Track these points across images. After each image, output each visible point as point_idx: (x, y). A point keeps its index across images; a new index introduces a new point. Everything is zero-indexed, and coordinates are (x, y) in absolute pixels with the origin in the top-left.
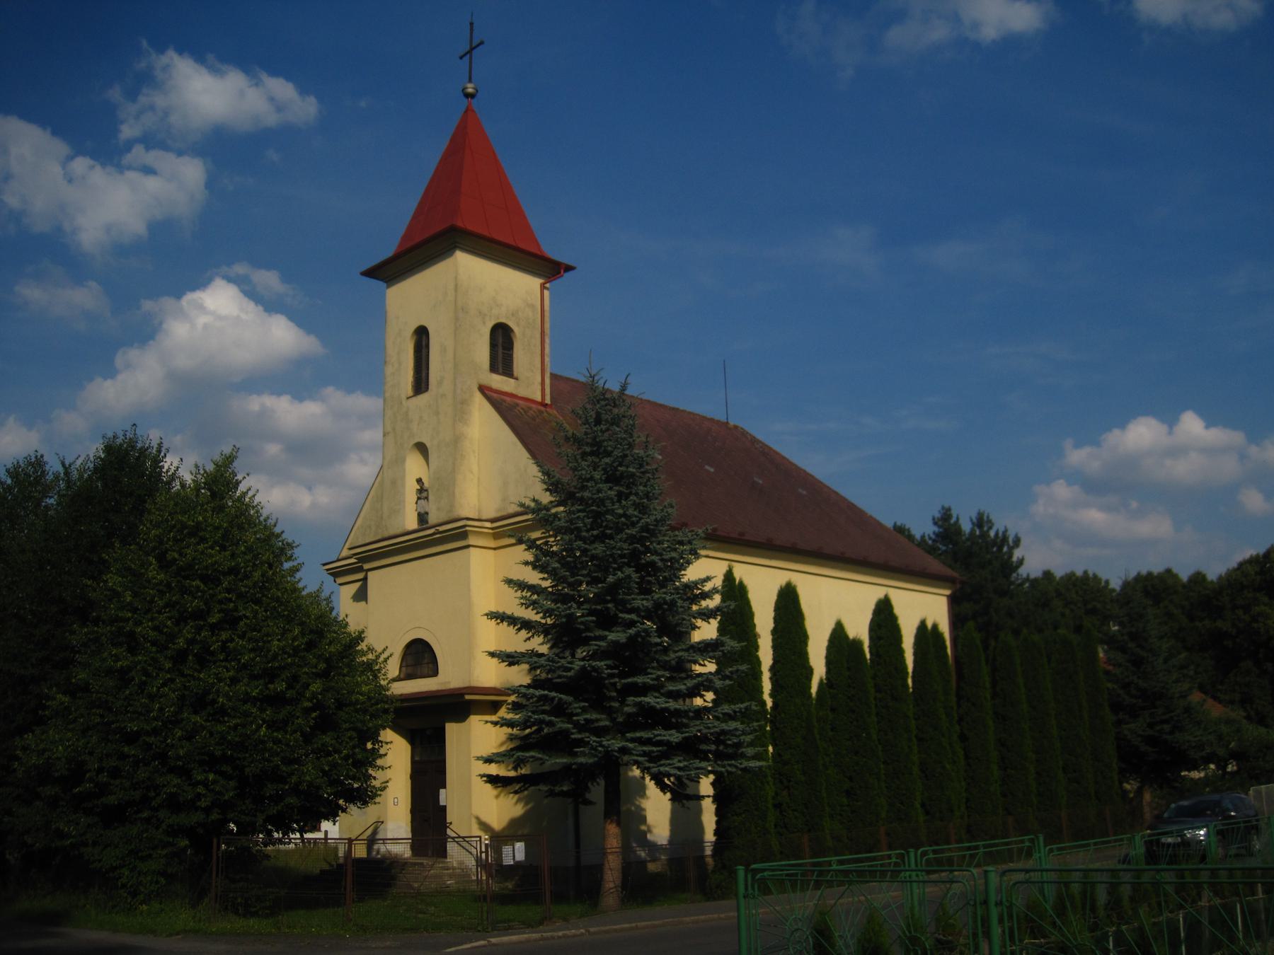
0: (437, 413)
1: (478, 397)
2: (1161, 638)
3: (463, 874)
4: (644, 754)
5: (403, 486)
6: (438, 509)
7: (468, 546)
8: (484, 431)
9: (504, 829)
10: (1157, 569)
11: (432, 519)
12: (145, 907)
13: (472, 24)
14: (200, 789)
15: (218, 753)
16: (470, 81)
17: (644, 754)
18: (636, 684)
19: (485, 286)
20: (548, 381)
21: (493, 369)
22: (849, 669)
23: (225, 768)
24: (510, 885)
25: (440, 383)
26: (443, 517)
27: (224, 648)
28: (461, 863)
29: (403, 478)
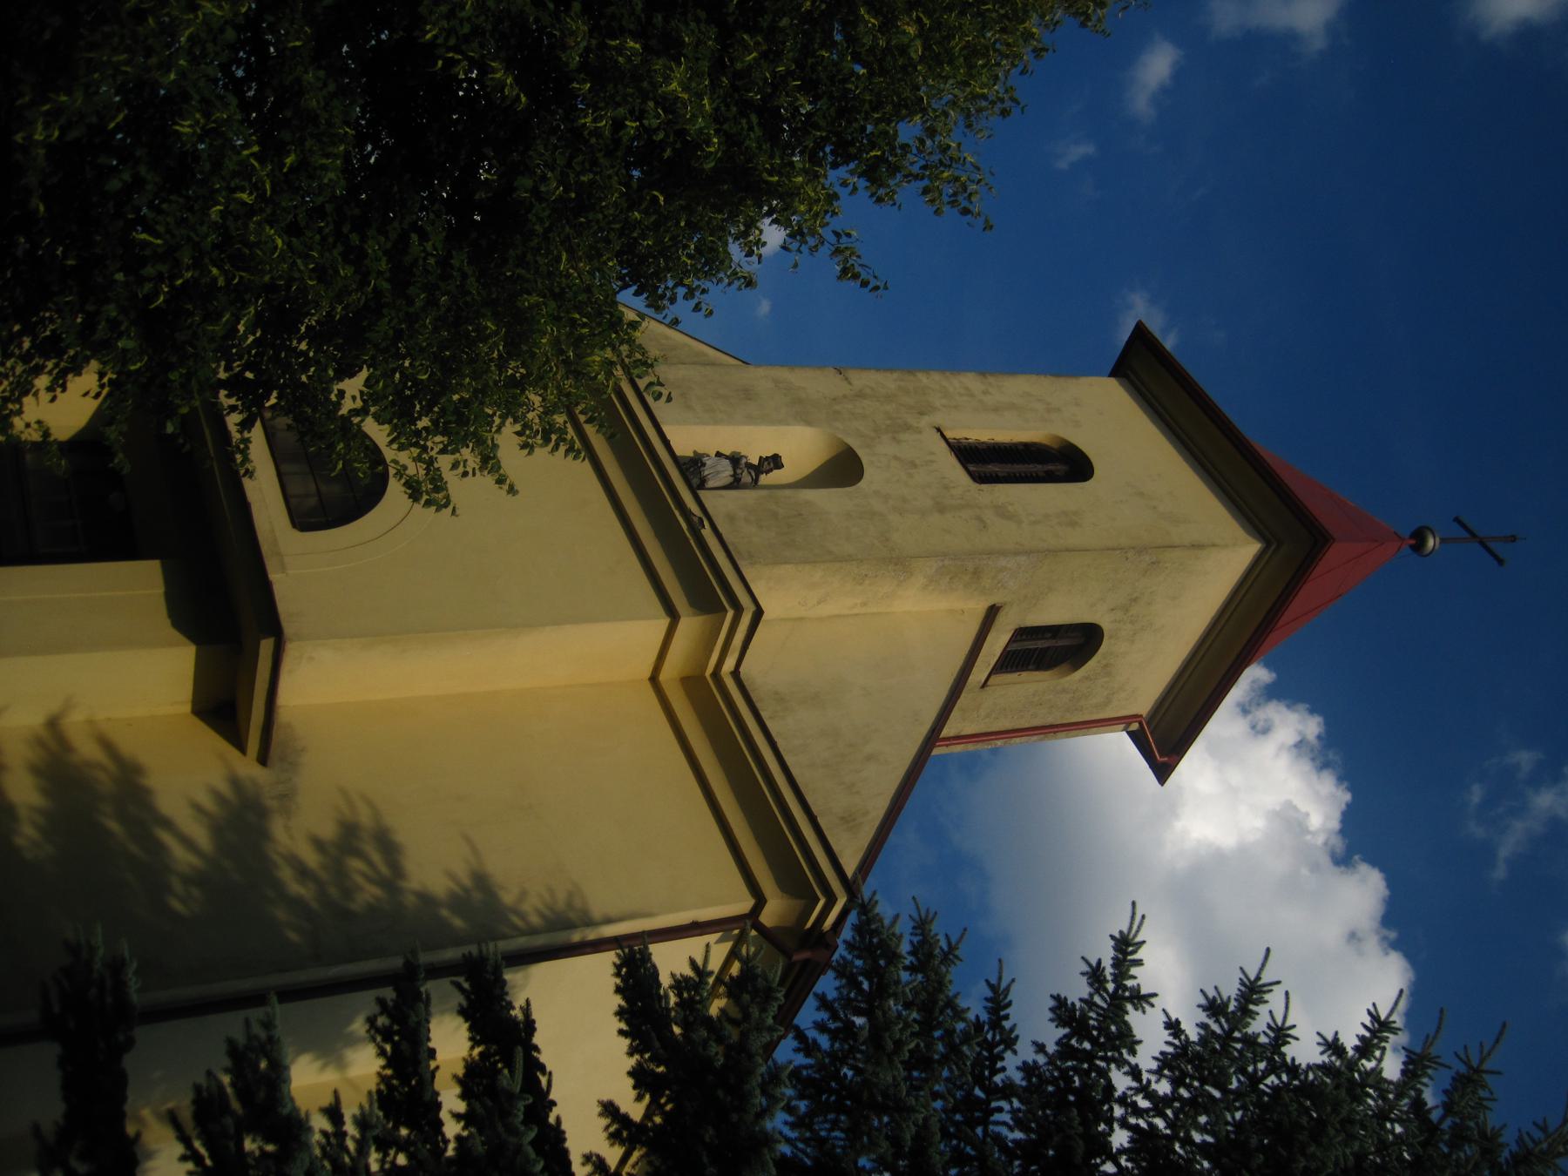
0: (941, 509)
1: (979, 607)
5: (750, 420)
7: (673, 614)
16: (1443, 541)
25: (1002, 512)
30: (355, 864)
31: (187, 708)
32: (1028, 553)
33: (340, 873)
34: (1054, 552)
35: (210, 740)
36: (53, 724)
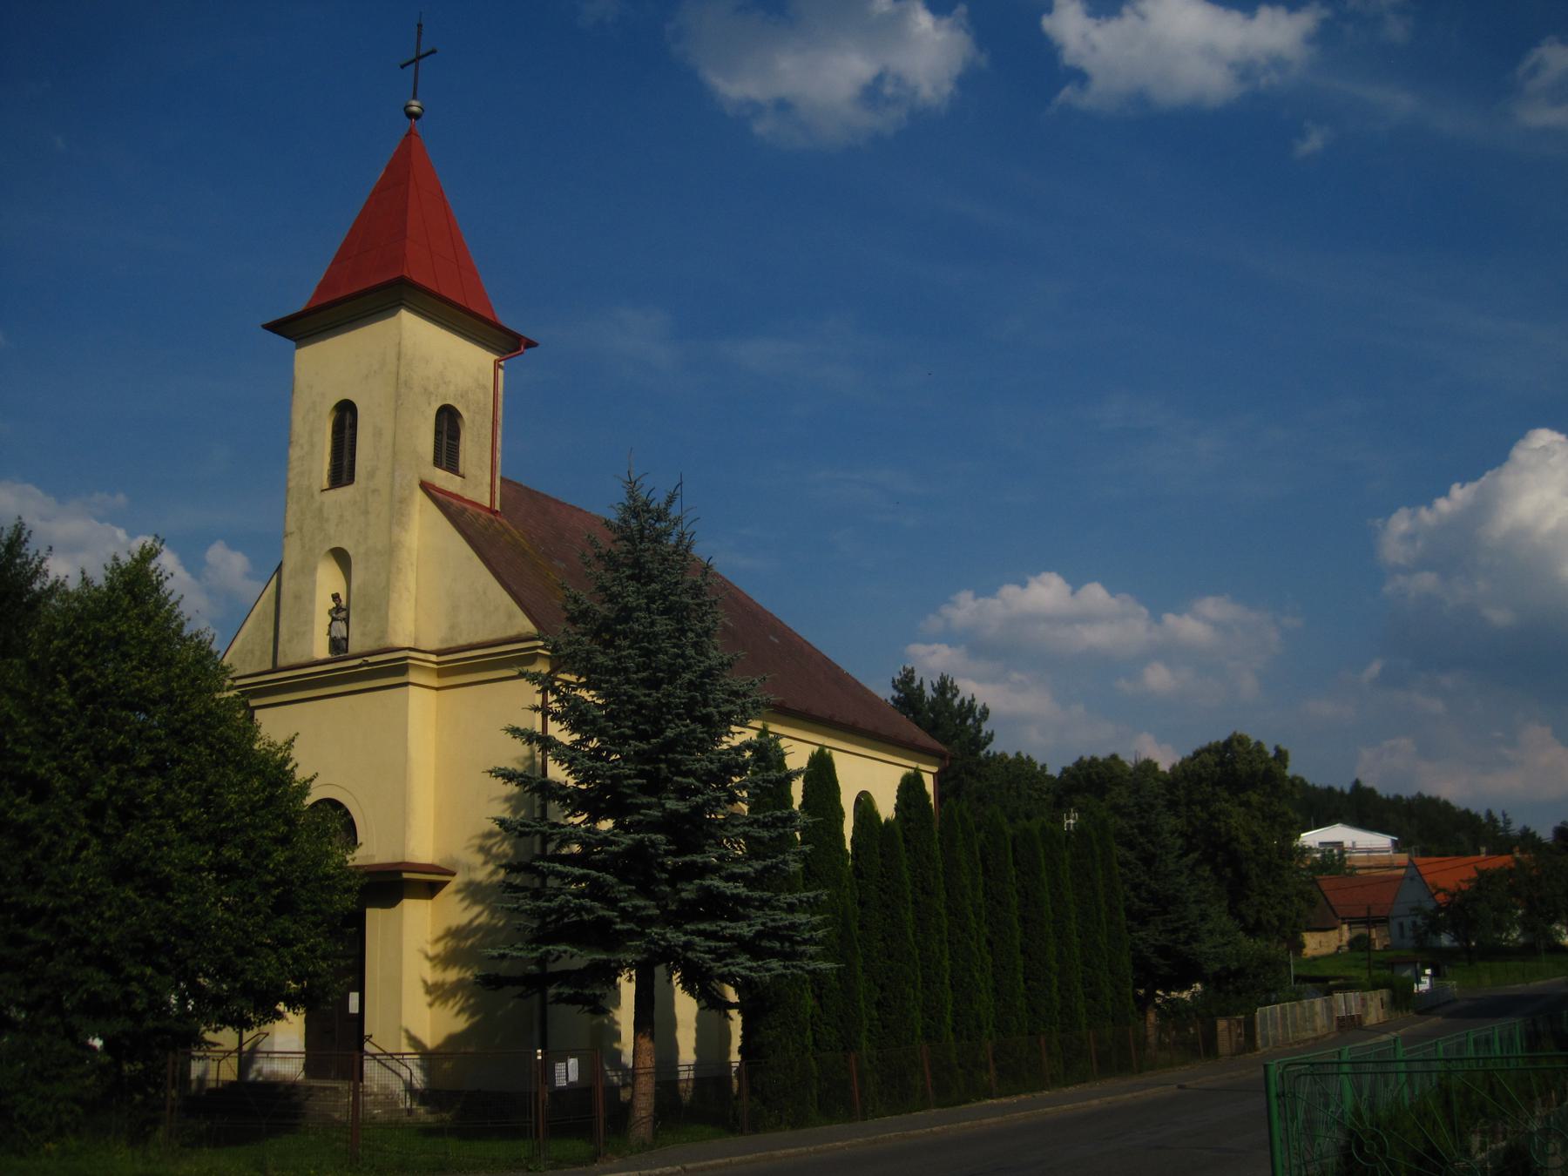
0: (366, 513)
1: (420, 495)
2: (1172, 833)
3: (389, 1100)
4: (710, 951)
5: (312, 601)
6: (363, 634)
7: (406, 684)
8: (426, 538)
9: (439, 1047)
10: (1102, 754)
11: (355, 646)
12: (51, 1146)
13: (420, 26)
14: (134, 987)
15: (159, 939)
16: (415, 98)
17: (710, 951)
18: (694, 863)
19: (424, 360)
20: (498, 482)
21: (437, 462)
22: (882, 855)
23: (163, 960)
24: (447, 1116)
25: (371, 475)
26: (371, 645)
27: (159, 800)
28: (386, 1087)
29: (312, 592)
30: (494, 850)
31: (430, 902)
32: (393, 471)
33: (497, 857)
34: (394, 454)
35: (441, 895)
36: (427, 957)
